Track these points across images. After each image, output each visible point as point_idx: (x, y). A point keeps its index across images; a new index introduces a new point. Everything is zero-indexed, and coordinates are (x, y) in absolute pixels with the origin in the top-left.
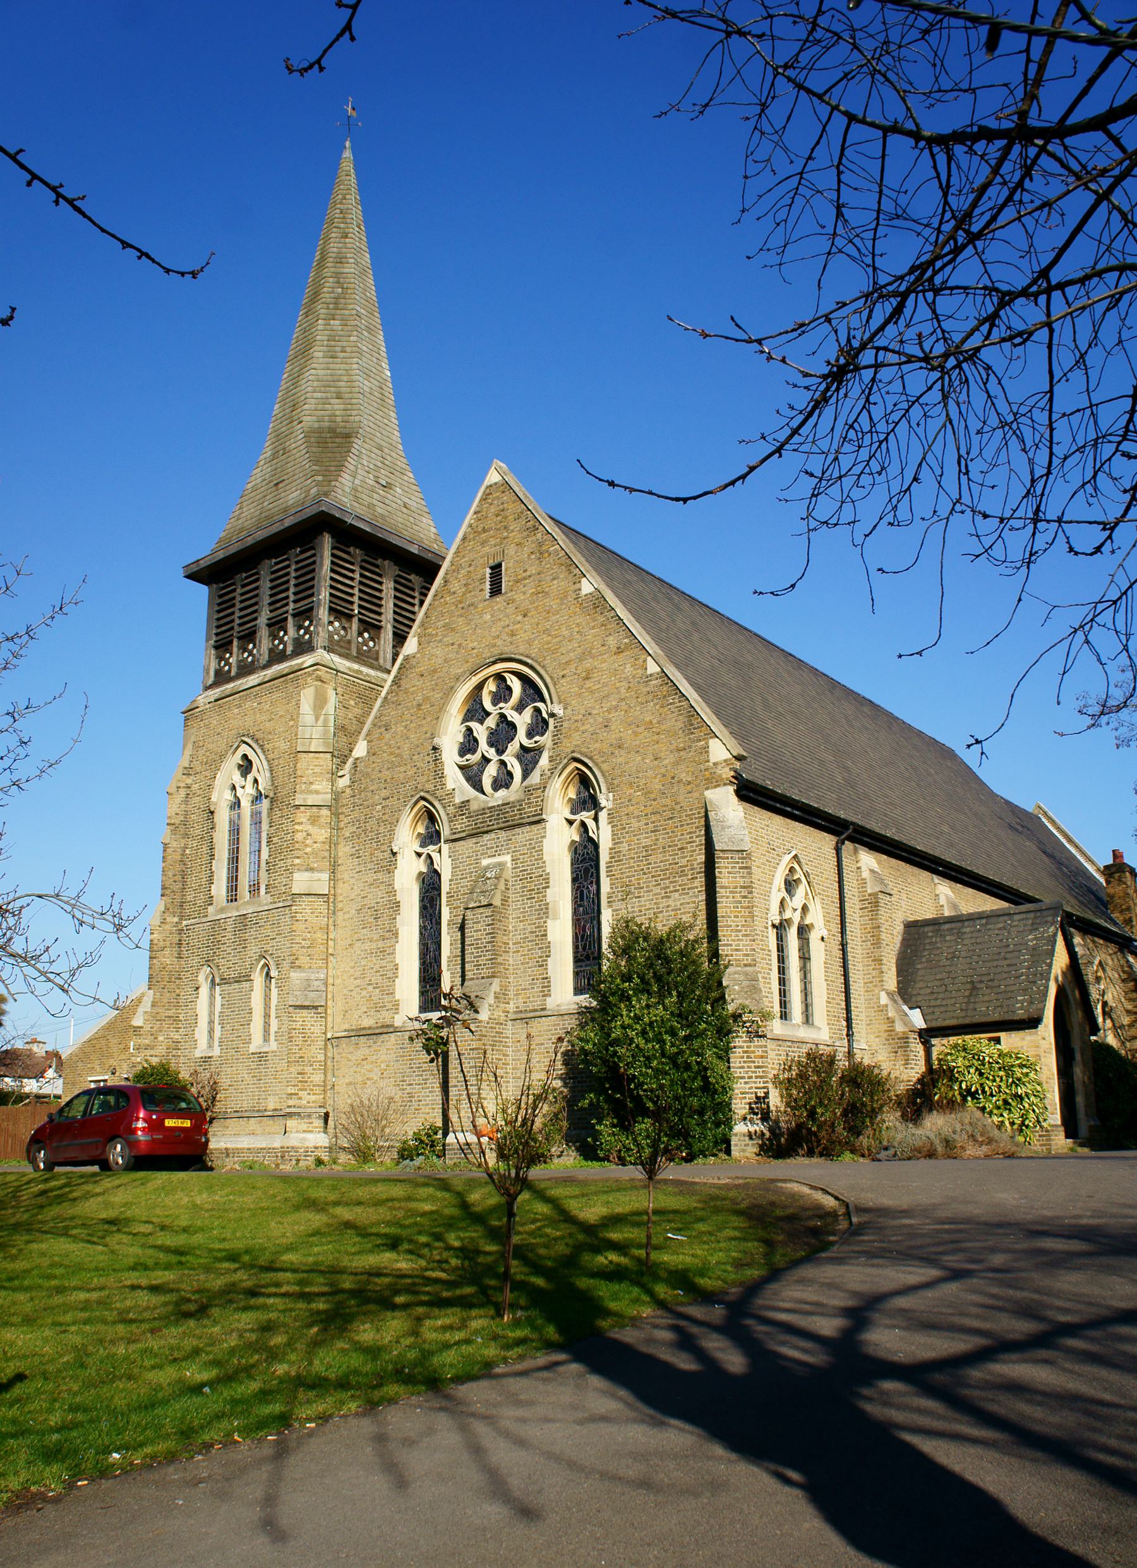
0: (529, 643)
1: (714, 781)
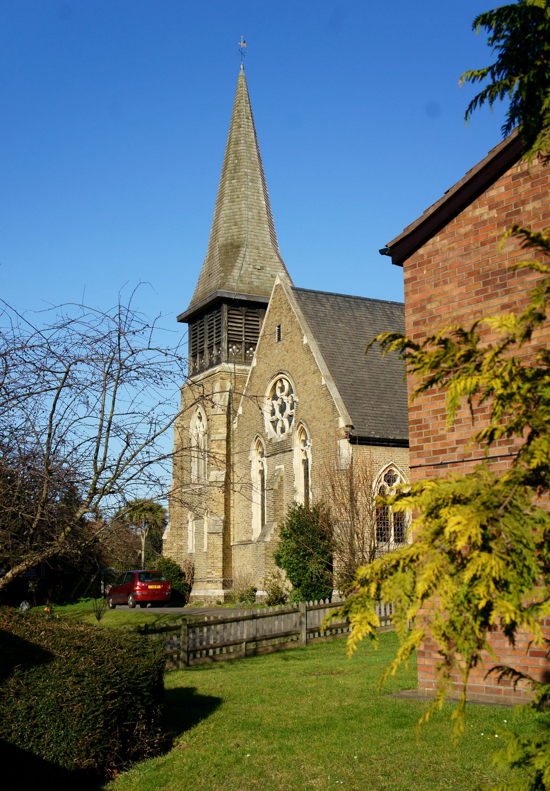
0: (289, 365)
1: (339, 437)
